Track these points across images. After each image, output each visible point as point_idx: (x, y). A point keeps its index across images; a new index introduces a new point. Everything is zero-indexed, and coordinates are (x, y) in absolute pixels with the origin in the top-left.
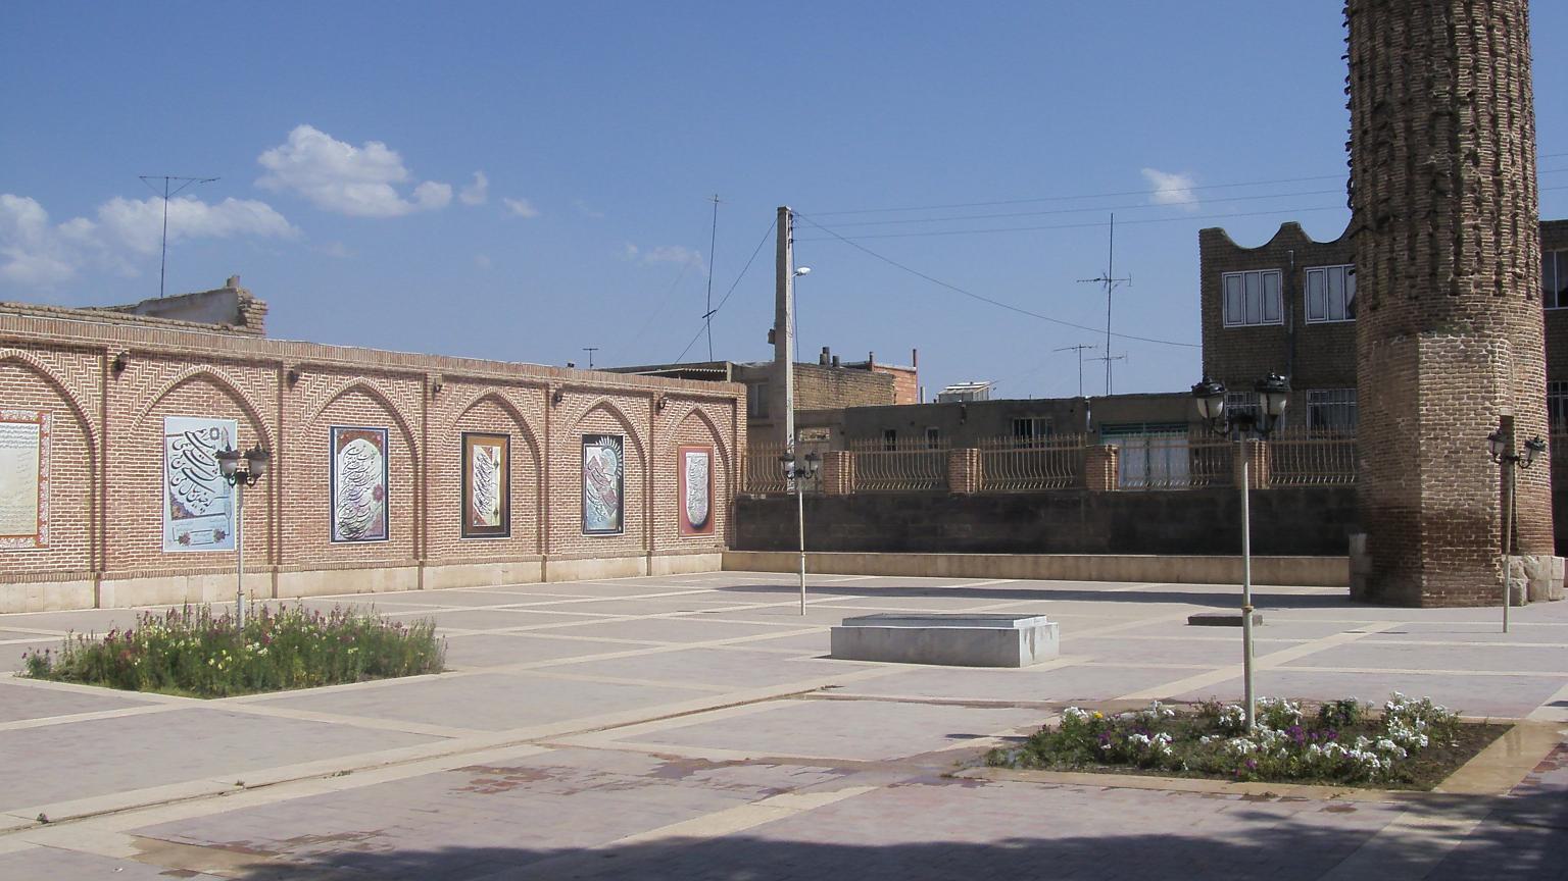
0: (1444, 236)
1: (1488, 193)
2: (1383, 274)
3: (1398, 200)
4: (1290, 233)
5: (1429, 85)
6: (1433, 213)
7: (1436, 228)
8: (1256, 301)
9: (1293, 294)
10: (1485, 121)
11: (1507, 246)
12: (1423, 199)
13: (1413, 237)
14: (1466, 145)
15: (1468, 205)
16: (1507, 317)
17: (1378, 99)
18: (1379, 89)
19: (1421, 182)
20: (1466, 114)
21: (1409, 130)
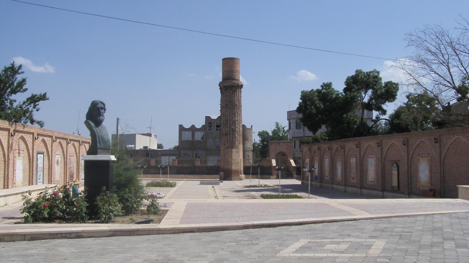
0: (234, 137)
1: (238, 132)
2: (226, 141)
3: (228, 132)
4: (193, 126)
5: (233, 118)
6: (232, 134)
7: (233, 136)
8: (188, 136)
9: (193, 136)
10: (238, 123)
11: (240, 138)
12: (231, 132)
13: (230, 137)
14: (236, 126)
15: (236, 133)
16: (240, 147)
17: (226, 119)
18: (226, 118)
19: (231, 130)
20: (236, 122)
21: (230, 124)
